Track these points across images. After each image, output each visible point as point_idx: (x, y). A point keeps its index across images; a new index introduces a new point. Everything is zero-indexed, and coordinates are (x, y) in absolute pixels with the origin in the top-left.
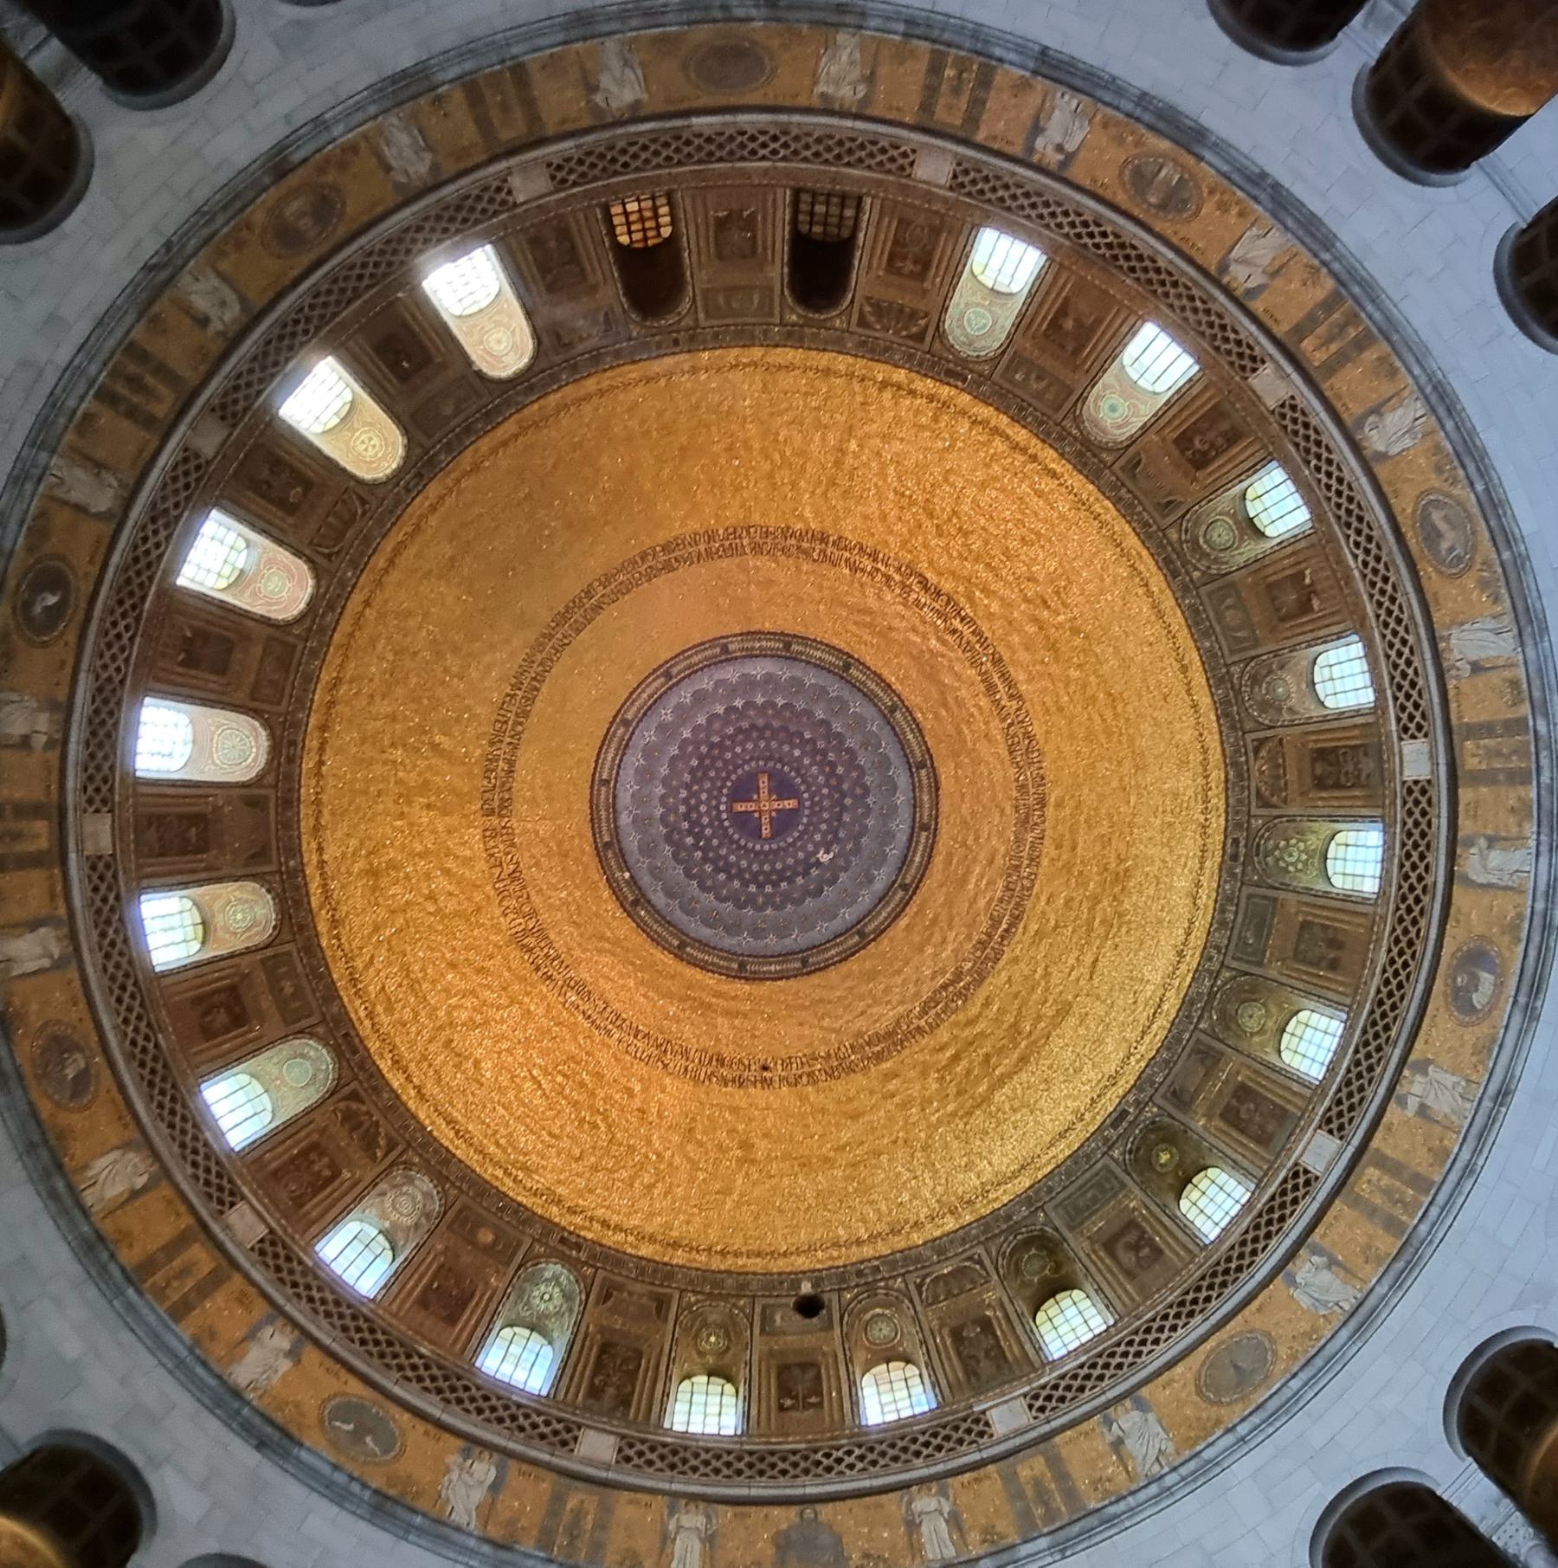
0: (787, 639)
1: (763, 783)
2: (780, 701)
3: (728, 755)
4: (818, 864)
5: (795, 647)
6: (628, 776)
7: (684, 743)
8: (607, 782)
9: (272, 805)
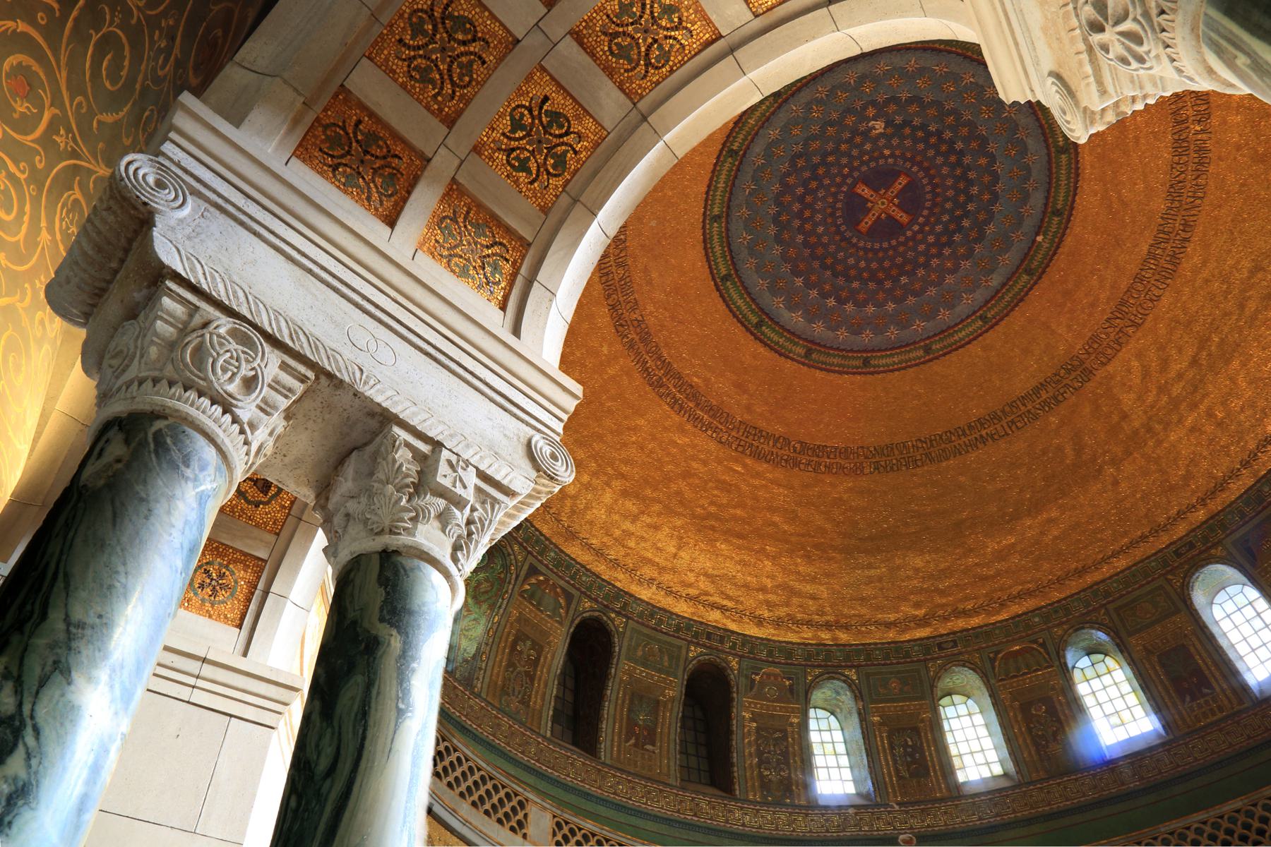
0: (754, 331)
1: (867, 222)
2: (799, 282)
3: (874, 265)
4: (889, 123)
5: (754, 320)
6: (962, 308)
7: (899, 301)
8: (982, 318)
9: (1237, 535)
